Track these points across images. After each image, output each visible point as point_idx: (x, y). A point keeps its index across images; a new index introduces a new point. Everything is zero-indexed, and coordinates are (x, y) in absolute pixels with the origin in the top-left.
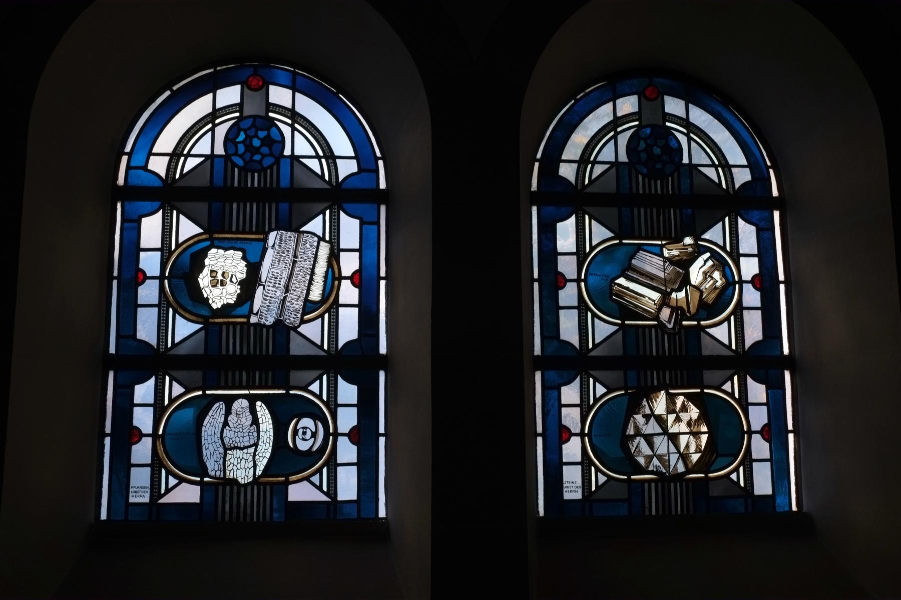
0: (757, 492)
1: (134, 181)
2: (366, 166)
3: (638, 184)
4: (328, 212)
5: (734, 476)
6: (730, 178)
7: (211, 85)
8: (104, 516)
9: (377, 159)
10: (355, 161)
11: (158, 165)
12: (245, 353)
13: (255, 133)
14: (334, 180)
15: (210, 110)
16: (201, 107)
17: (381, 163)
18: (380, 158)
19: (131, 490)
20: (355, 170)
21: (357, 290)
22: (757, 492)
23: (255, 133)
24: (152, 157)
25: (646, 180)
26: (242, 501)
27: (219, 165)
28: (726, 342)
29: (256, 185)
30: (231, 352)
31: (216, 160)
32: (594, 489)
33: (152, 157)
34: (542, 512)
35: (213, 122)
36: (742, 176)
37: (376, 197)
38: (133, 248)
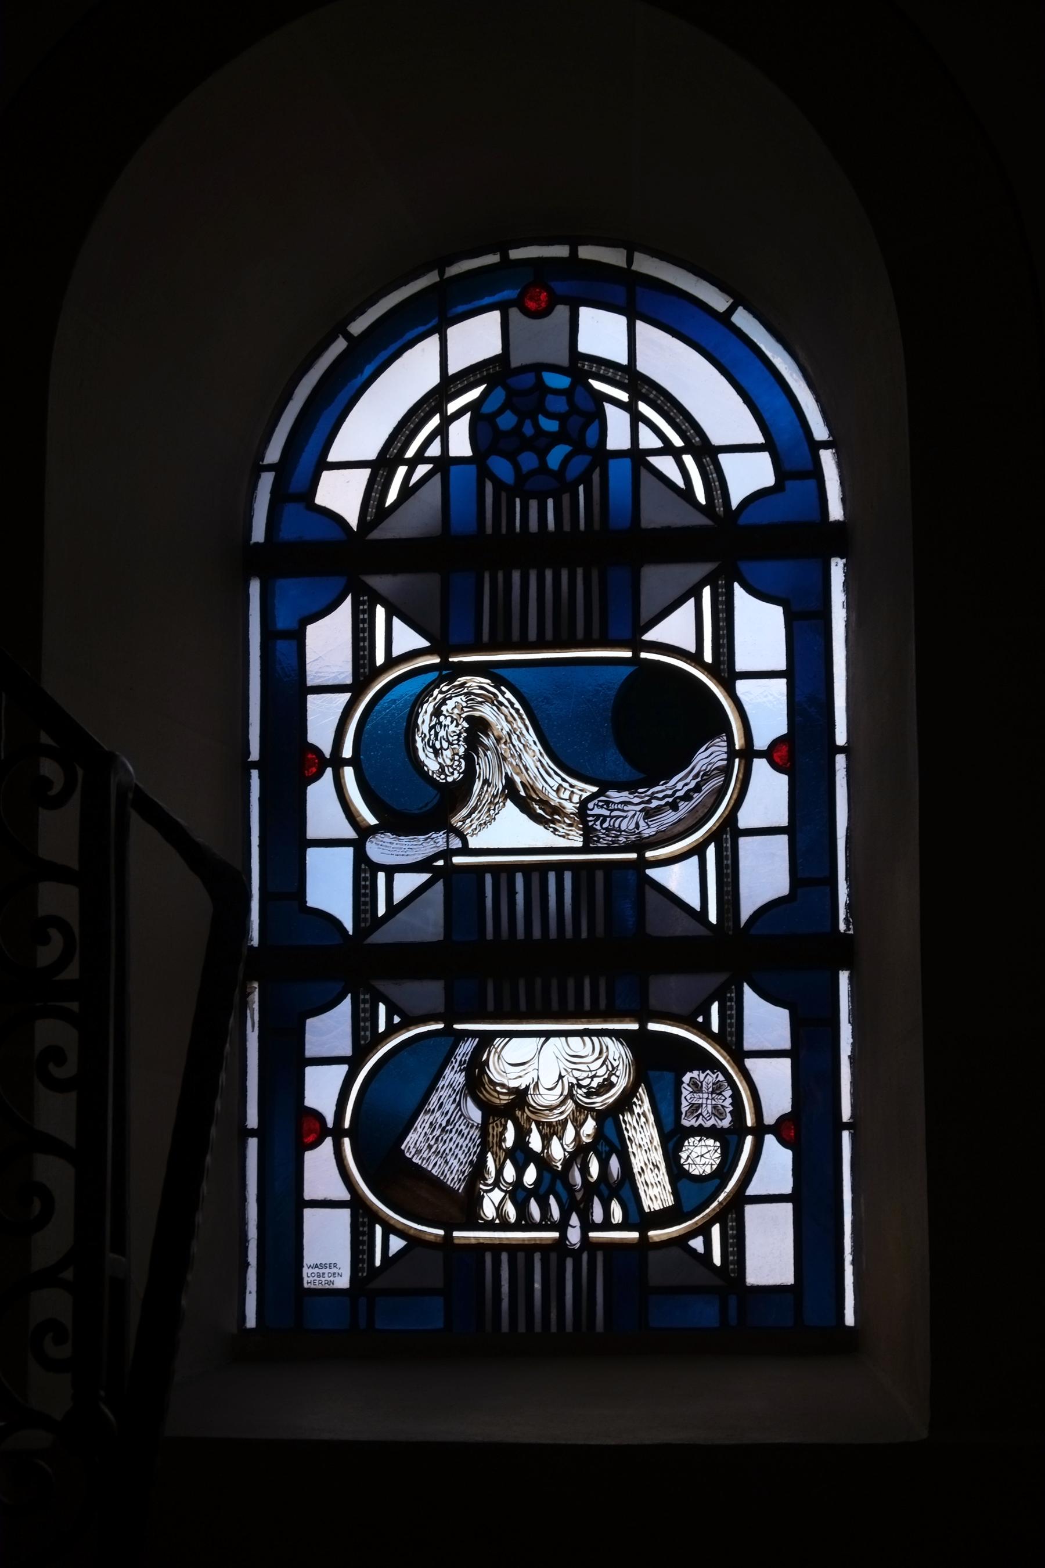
1: (288, 532)
2: (795, 464)
3: (512, 893)
4: (707, 592)
6: (716, 481)
7: (436, 315)
8: (251, 1322)
9: (816, 446)
10: (765, 457)
11: (341, 494)
12: (537, 934)
13: (536, 410)
14: (720, 510)
15: (434, 379)
16: (414, 373)
18: (825, 445)
19: (305, 1270)
20: (768, 479)
21: (784, 779)
23: (536, 410)
24: (326, 475)
25: (504, 495)
26: (553, 1316)
27: (463, 479)
30: (521, 933)
31: (454, 470)
33: (326, 475)
35: (441, 409)
36: (749, 475)
37: (824, 540)
38: (289, 690)
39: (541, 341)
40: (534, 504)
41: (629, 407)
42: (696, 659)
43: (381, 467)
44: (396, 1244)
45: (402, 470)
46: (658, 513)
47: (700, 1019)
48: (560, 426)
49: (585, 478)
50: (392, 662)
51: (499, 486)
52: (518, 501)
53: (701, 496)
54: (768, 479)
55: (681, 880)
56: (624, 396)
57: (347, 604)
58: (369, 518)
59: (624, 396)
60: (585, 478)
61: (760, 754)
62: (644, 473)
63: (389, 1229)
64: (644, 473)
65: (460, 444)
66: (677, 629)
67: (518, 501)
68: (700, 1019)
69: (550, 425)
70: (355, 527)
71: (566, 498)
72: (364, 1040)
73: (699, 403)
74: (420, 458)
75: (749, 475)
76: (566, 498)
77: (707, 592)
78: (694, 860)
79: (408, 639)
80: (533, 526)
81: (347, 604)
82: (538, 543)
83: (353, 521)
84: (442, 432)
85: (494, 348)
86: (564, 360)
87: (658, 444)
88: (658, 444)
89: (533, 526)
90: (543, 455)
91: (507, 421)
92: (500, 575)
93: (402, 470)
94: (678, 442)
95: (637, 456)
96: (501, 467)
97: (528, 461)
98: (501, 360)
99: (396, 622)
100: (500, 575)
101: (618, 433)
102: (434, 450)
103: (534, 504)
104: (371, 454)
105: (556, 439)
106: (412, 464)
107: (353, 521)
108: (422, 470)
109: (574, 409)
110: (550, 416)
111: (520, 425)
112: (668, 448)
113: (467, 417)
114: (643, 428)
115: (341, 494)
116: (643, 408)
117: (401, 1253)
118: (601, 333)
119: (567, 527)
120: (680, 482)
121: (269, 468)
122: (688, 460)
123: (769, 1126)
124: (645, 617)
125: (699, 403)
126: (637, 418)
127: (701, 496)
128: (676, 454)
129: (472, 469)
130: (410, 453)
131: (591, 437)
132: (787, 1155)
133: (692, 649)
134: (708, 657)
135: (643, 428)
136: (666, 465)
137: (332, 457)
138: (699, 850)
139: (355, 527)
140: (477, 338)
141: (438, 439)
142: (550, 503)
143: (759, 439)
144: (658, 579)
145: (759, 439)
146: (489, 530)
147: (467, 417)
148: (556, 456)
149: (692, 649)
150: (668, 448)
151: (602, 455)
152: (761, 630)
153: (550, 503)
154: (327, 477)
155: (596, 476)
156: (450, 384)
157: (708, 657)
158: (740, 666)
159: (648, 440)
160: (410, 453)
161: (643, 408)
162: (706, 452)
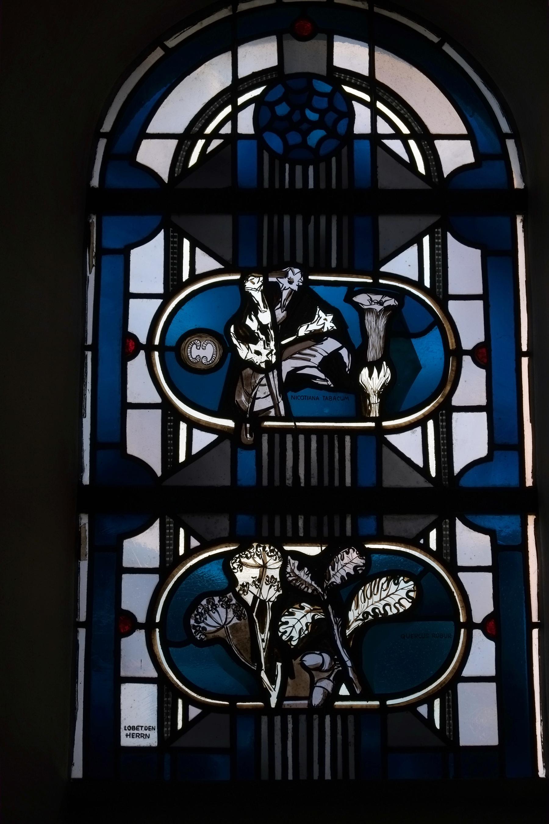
0: (467, 739)
5: (423, 710)
6: (432, 158)
11: (156, 156)
13: (302, 101)
17: (511, 144)
18: (509, 136)
20: (470, 158)
22: (467, 739)
23: (302, 101)
25: (277, 162)
28: (420, 462)
29: (311, 185)
31: (241, 144)
32: (180, 726)
34: (77, 772)
36: (455, 155)
39: (305, 57)
40: (299, 169)
41: (371, 106)
42: (419, 285)
43: (186, 140)
44: (194, 712)
45: (201, 143)
46: (389, 179)
47: (422, 541)
48: (320, 118)
49: (337, 152)
50: (194, 278)
51: (273, 155)
52: (287, 166)
53: (421, 168)
54: (470, 158)
55: (408, 444)
56: (367, 98)
57: (161, 236)
58: (176, 175)
59: (367, 98)
60: (337, 152)
61: (467, 353)
62: (379, 149)
63: (188, 701)
64: (379, 149)
65: (246, 123)
66: (404, 264)
67: (287, 166)
68: (422, 541)
69: (312, 116)
70: (166, 181)
71: (322, 166)
72: (169, 560)
73: (421, 116)
74: (216, 134)
75: (455, 155)
76: (322, 166)
77: (426, 240)
78: (419, 430)
79: (206, 263)
80: (299, 185)
81: (161, 236)
82: (301, 196)
83: (165, 175)
84: (232, 118)
85: (272, 61)
86: (322, 70)
87: (391, 131)
88: (391, 131)
89: (299, 185)
90: (305, 134)
91: (282, 109)
92: (276, 219)
93: (201, 143)
94: (405, 130)
95: (375, 138)
96: (274, 142)
97: (294, 138)
98: (279, 69)
99: (198, 250)
100: (276, 219)
101: (362, 122)
102: (227, 129)
103: (299, 169)
104: (180, 129)
105: (315, 125)
106: (209, 139)
107: (165, 175)
108: (215, 143)
109: (331, 107)
110: (314, 110)
111: (290, 114)
112: (398, 135)
113: (252, 107)
114: (379, 119)
115: (156, 156)
116: (380, 105)
117: (198, 718)
118: (350, 55)
119: (323, 186)
120: (406, 157)
121: (104, 135)
122: (412, 143)
123: (83, 622)
124: (382, 254)
125: (421, 116)
126: (375, 113)
127: (421, 168)
128: (404, 139)
129: (254, 143)
130: (209, 130)
131: (342, 127)
132: (491, 645)
133: (415, 278)
134: (427, 283)
135: (379, 119)
136: (396, 146)
137: (151, 130)
138: (422, 423)
139: (166, 181)
140: (259, 56)
141: (230, 123)
142: (311, 169)
143: (464, 131)
144: (389, 226)
145: (464, 131)
146: (266, 185)
147: (252, 107)
148: (316, 135)
149: (415, 278)
150: (398, 135)
151: (351, 137)
152: (465, 266)
153: (311, 169)
154: (146, 144)
155: (345, 151)
156: (238, 85)
157: (427, 283)
158: (452, 290)
159: (383, 128)
160: (209, 130)
161: (380, 105)
162: (426, 139)
